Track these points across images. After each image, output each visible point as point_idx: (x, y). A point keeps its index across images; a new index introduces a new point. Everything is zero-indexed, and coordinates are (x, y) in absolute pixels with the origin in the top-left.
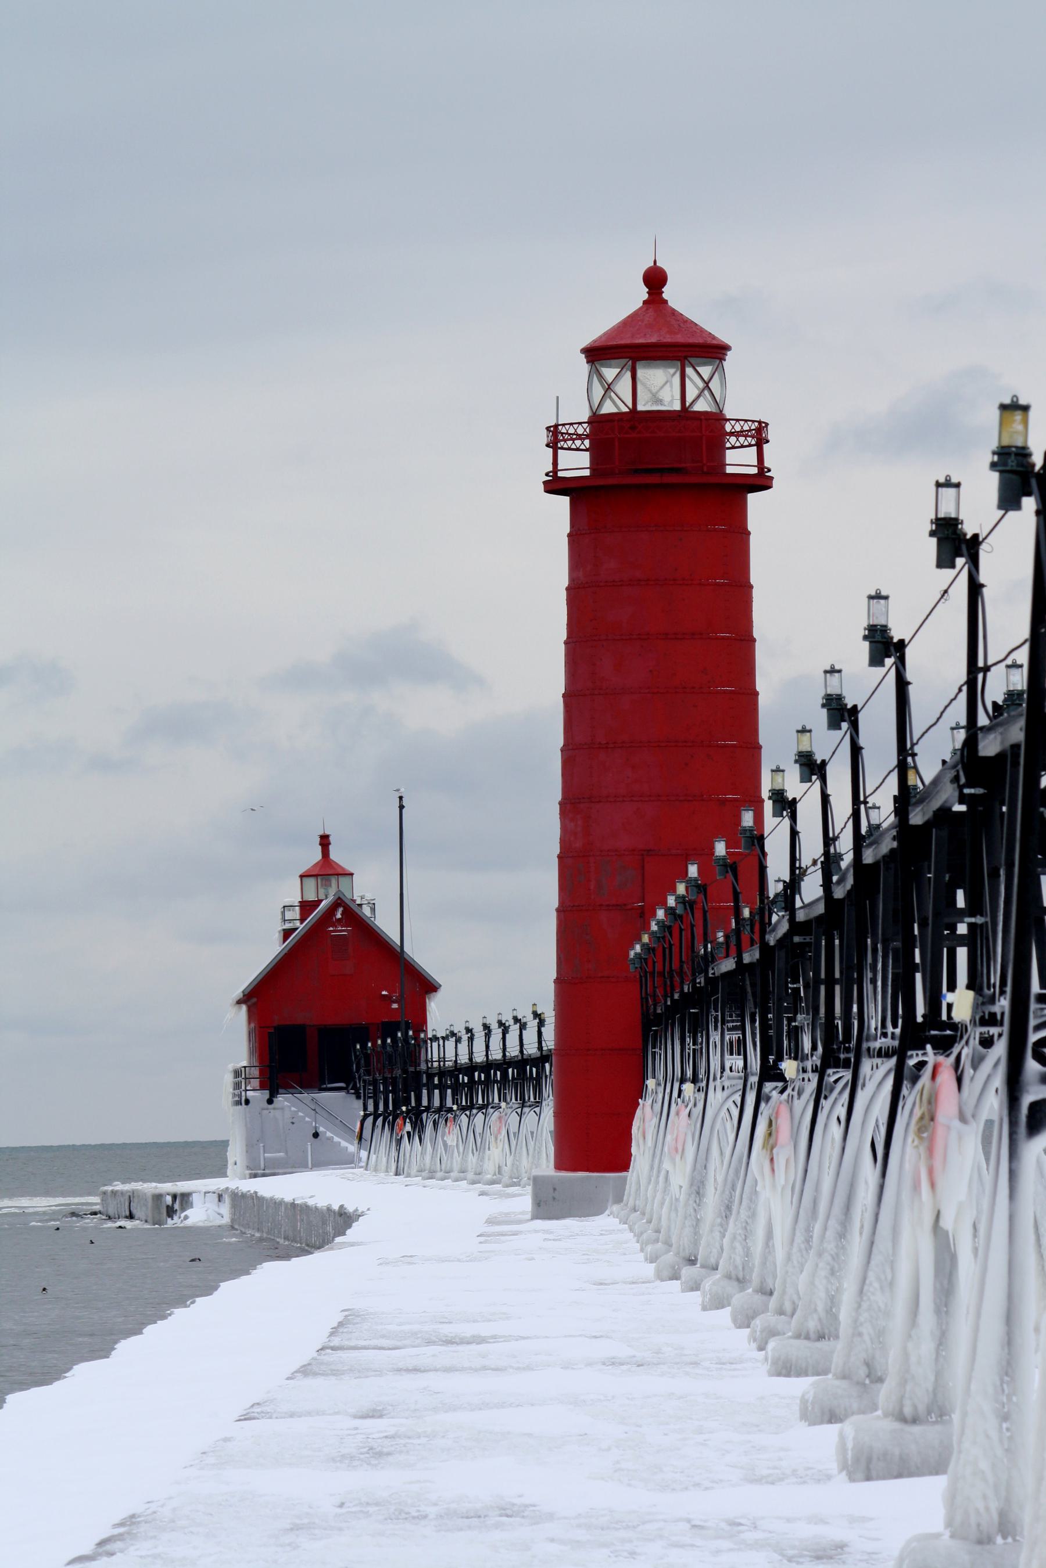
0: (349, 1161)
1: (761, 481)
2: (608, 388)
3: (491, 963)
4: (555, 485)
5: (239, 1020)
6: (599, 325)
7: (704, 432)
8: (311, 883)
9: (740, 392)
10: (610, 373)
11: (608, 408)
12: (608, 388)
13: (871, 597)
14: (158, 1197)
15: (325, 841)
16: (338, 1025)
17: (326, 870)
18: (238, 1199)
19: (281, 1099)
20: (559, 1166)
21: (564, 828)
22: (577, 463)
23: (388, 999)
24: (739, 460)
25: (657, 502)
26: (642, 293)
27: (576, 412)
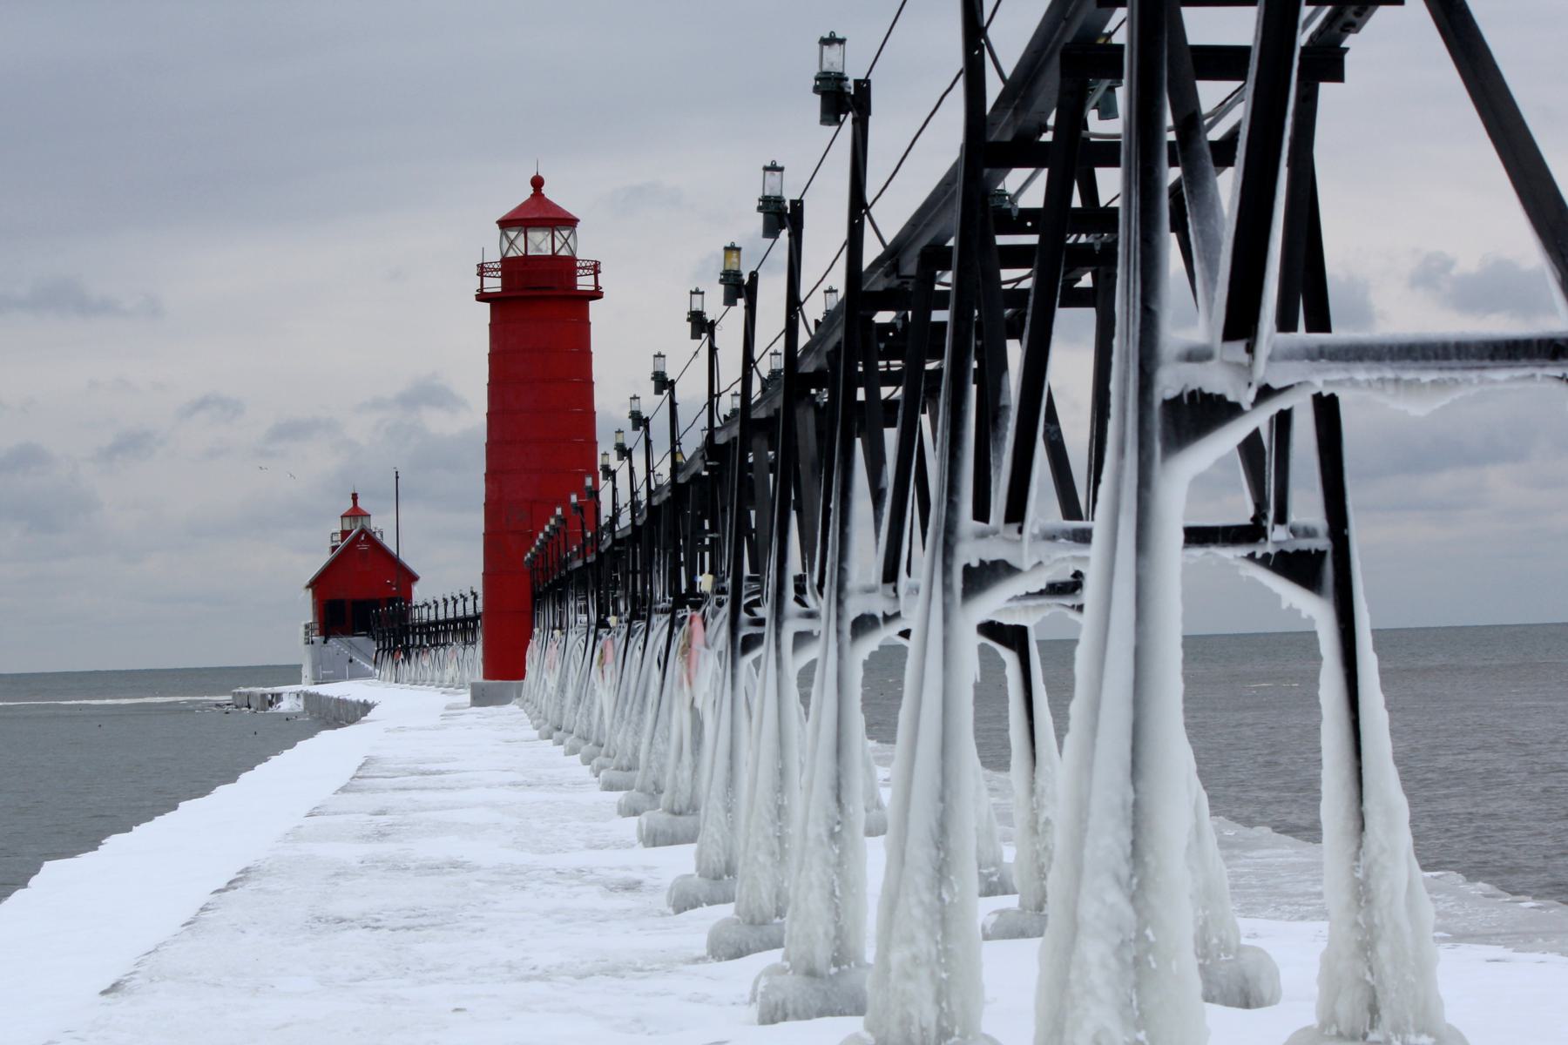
0: (369, 675)
1: (597, 294)
2: (512, 243)
3: (447, 563)
4: (482, 297)
5: (307, 598)
6: (506, 208)
7: (565, 267)
8: (347, 520)
9: (585, 245)
10: (512, 234)
11: (511, 254)
12: (512, 243)
13: (766, 169)
14: (264, 696)
15: (355, 497)
16: (363, 601)
17: (356, 513)
18: (309, 698)
19: (331, 641)
20: (487, 676)
21: (487, 488)
22: (494, 284)
23: (390, 585)
24: (584, 283)
25: (539, 307)
26: (531, 190)
27: (494, 256)
